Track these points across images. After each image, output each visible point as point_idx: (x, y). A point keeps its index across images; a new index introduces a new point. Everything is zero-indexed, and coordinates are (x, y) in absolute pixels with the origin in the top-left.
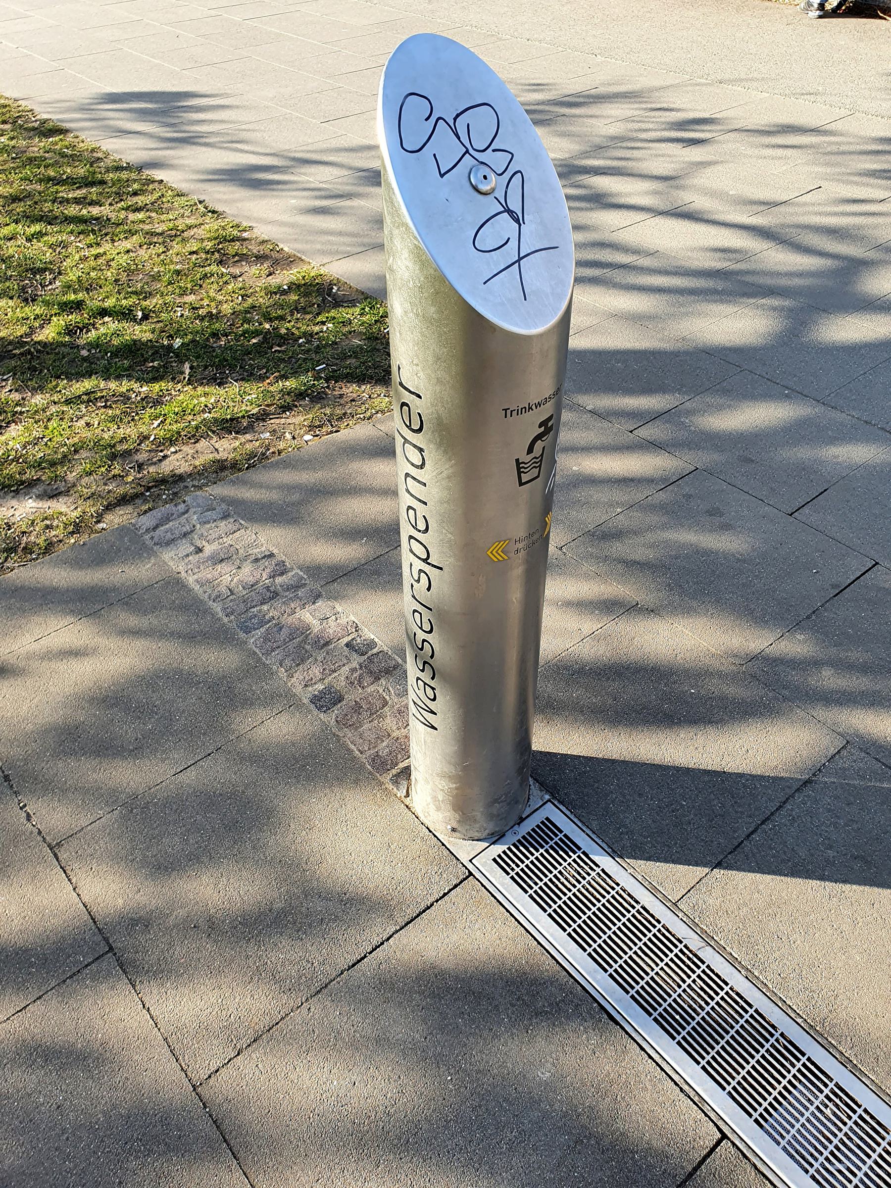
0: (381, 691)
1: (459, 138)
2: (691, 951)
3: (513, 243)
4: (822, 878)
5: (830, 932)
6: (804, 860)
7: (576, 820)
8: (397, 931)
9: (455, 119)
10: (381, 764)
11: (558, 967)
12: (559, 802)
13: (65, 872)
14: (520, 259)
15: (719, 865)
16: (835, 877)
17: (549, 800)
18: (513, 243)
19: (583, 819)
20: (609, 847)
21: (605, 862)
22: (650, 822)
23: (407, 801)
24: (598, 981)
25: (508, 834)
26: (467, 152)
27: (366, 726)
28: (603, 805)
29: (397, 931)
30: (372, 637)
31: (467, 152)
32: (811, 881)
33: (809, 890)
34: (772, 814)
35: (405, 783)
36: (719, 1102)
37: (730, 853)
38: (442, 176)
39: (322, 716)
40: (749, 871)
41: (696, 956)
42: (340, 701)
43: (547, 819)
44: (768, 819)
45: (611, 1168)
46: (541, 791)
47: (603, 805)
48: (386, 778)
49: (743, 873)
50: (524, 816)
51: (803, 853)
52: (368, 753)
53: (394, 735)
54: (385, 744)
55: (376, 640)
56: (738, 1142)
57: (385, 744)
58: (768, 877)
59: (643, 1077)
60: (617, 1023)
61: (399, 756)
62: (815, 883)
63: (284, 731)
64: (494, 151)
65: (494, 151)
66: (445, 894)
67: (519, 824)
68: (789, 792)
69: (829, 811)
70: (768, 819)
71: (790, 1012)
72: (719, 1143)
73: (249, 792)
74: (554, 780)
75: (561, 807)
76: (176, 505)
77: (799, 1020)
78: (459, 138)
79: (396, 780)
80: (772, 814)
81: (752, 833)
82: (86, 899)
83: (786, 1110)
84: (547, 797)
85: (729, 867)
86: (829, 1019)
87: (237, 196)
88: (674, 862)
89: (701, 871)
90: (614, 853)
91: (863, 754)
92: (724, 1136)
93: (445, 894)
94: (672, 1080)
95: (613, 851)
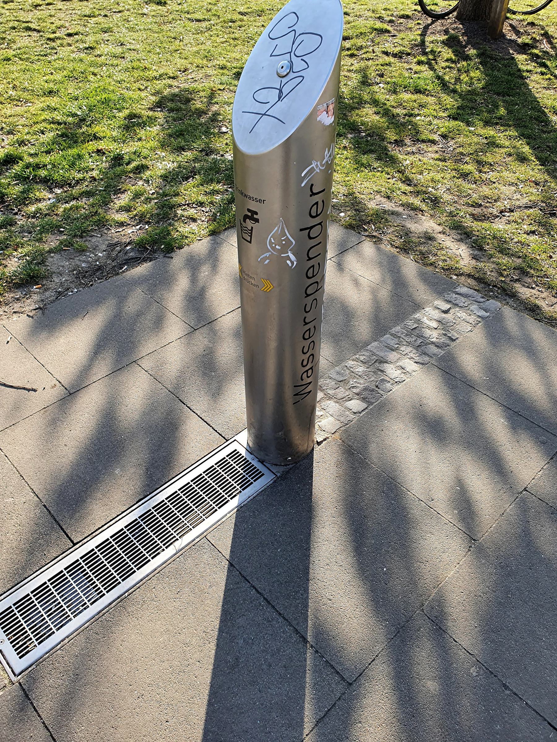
1: (293, 44)
2: (174, 541)
3: (268, 106)
4: (221, 630)
5: (180, 625)
6: (235, 621)
8: (197, 414)
9: (300, 35)
11: (171, 478)
12: (275, 481)
14: (265, 114)
15: (231, 565)
16: (221, 640)
17: (276, 476)
18: (268, 106)
19: (263, 492)
20: (244, 505)
21: (234, 503)
22: (263, 528)
24: (162, 496)
25: (252, 456)
26: (290, 53)
28: (274, 503)
29: (197, 414)
31: (290, 53)
32: (218, 622)
33: (211, 619)
34: (273, 607)
36: (92, 544)
37: (240, 573)
38: (271, 56)
40: (226, 583)
41: (172, 543)
43: (263, 474)
44: (268, 602)
45: (71, 496)
47: (274, 503)
49: (225, 579)
50: (264, 463)
51: (241, 621)
56: (71, 550)
58: (222, 595)
59: (109, 512)
60: (137, 502)
62: (217, 623)
64: (302, 60)
65: (302, 60)
66: (216, 431)
67: (259, 461)
68: (294, 623)
69: (279, 650)
70: (268, 602)
71: (133, 590)
72: (72, 542)
77: (126, 594)
78: (293, 44)
80: (273, 607)
81: (256, 590)
83: (81, 578)
84: (279, 475)
85: (229, 571)
86: (124, 610)
88: (233, 539)
89: (227, 553)
90: (240, 509)
91: (338, 695)
92: (75, 544)
93: (216, 431)
94: (105, 524)
95: (242, 507)
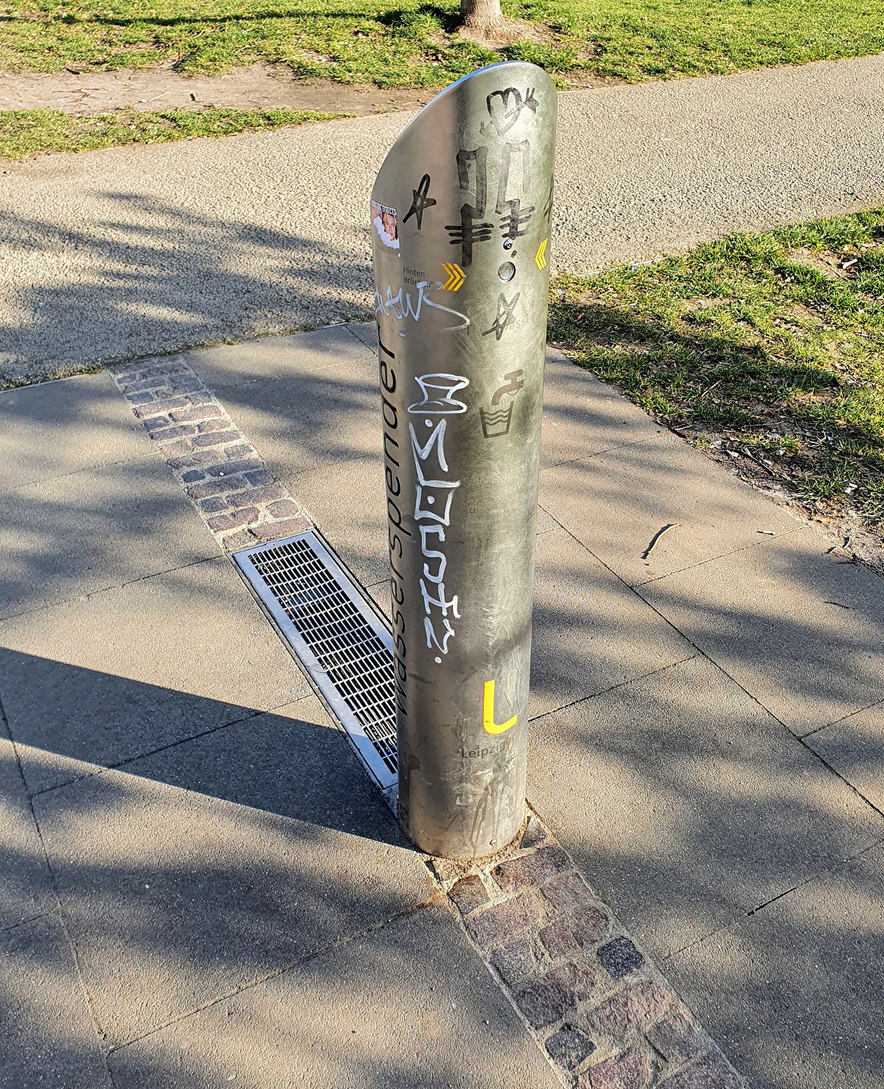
0: (547, 955)
7: (367, 767)
10: (557, 858)
12: (374, 784)
13: (872, 805)
21: (355, 729)
23: (530, 813)
27: (570, 911)
30: (551, 1062)
35: (530, 829)
39: (626, 934)
42: (603, 948)
46: (388, 799)
48: (549, 840)
52: (569, 873)
53: (534, 890)
54: (548, 880)
55: (546, 1055)
57: (548, 880)
61: (533, 861)
63: (672, 921)
73: (702, 853)
74: (370, 805)
75: (374, 780)
76: (814, 908)
79: (540, 835)
82: (839, 780)
84: (385, 792)
87: (281, 709)
90: (344, 736)
